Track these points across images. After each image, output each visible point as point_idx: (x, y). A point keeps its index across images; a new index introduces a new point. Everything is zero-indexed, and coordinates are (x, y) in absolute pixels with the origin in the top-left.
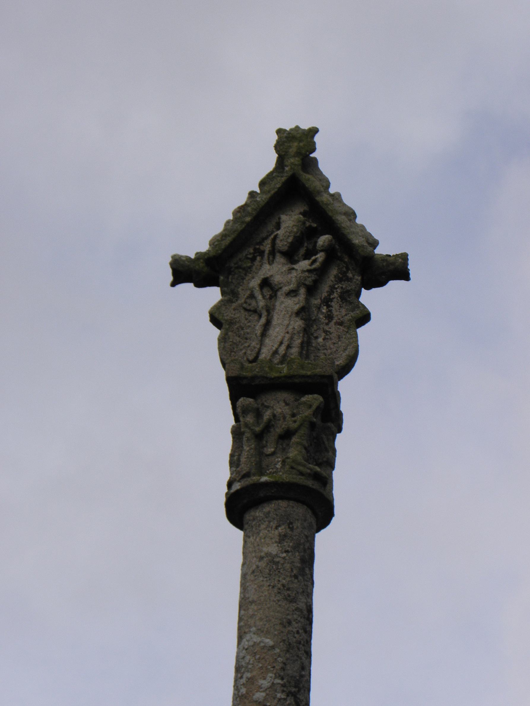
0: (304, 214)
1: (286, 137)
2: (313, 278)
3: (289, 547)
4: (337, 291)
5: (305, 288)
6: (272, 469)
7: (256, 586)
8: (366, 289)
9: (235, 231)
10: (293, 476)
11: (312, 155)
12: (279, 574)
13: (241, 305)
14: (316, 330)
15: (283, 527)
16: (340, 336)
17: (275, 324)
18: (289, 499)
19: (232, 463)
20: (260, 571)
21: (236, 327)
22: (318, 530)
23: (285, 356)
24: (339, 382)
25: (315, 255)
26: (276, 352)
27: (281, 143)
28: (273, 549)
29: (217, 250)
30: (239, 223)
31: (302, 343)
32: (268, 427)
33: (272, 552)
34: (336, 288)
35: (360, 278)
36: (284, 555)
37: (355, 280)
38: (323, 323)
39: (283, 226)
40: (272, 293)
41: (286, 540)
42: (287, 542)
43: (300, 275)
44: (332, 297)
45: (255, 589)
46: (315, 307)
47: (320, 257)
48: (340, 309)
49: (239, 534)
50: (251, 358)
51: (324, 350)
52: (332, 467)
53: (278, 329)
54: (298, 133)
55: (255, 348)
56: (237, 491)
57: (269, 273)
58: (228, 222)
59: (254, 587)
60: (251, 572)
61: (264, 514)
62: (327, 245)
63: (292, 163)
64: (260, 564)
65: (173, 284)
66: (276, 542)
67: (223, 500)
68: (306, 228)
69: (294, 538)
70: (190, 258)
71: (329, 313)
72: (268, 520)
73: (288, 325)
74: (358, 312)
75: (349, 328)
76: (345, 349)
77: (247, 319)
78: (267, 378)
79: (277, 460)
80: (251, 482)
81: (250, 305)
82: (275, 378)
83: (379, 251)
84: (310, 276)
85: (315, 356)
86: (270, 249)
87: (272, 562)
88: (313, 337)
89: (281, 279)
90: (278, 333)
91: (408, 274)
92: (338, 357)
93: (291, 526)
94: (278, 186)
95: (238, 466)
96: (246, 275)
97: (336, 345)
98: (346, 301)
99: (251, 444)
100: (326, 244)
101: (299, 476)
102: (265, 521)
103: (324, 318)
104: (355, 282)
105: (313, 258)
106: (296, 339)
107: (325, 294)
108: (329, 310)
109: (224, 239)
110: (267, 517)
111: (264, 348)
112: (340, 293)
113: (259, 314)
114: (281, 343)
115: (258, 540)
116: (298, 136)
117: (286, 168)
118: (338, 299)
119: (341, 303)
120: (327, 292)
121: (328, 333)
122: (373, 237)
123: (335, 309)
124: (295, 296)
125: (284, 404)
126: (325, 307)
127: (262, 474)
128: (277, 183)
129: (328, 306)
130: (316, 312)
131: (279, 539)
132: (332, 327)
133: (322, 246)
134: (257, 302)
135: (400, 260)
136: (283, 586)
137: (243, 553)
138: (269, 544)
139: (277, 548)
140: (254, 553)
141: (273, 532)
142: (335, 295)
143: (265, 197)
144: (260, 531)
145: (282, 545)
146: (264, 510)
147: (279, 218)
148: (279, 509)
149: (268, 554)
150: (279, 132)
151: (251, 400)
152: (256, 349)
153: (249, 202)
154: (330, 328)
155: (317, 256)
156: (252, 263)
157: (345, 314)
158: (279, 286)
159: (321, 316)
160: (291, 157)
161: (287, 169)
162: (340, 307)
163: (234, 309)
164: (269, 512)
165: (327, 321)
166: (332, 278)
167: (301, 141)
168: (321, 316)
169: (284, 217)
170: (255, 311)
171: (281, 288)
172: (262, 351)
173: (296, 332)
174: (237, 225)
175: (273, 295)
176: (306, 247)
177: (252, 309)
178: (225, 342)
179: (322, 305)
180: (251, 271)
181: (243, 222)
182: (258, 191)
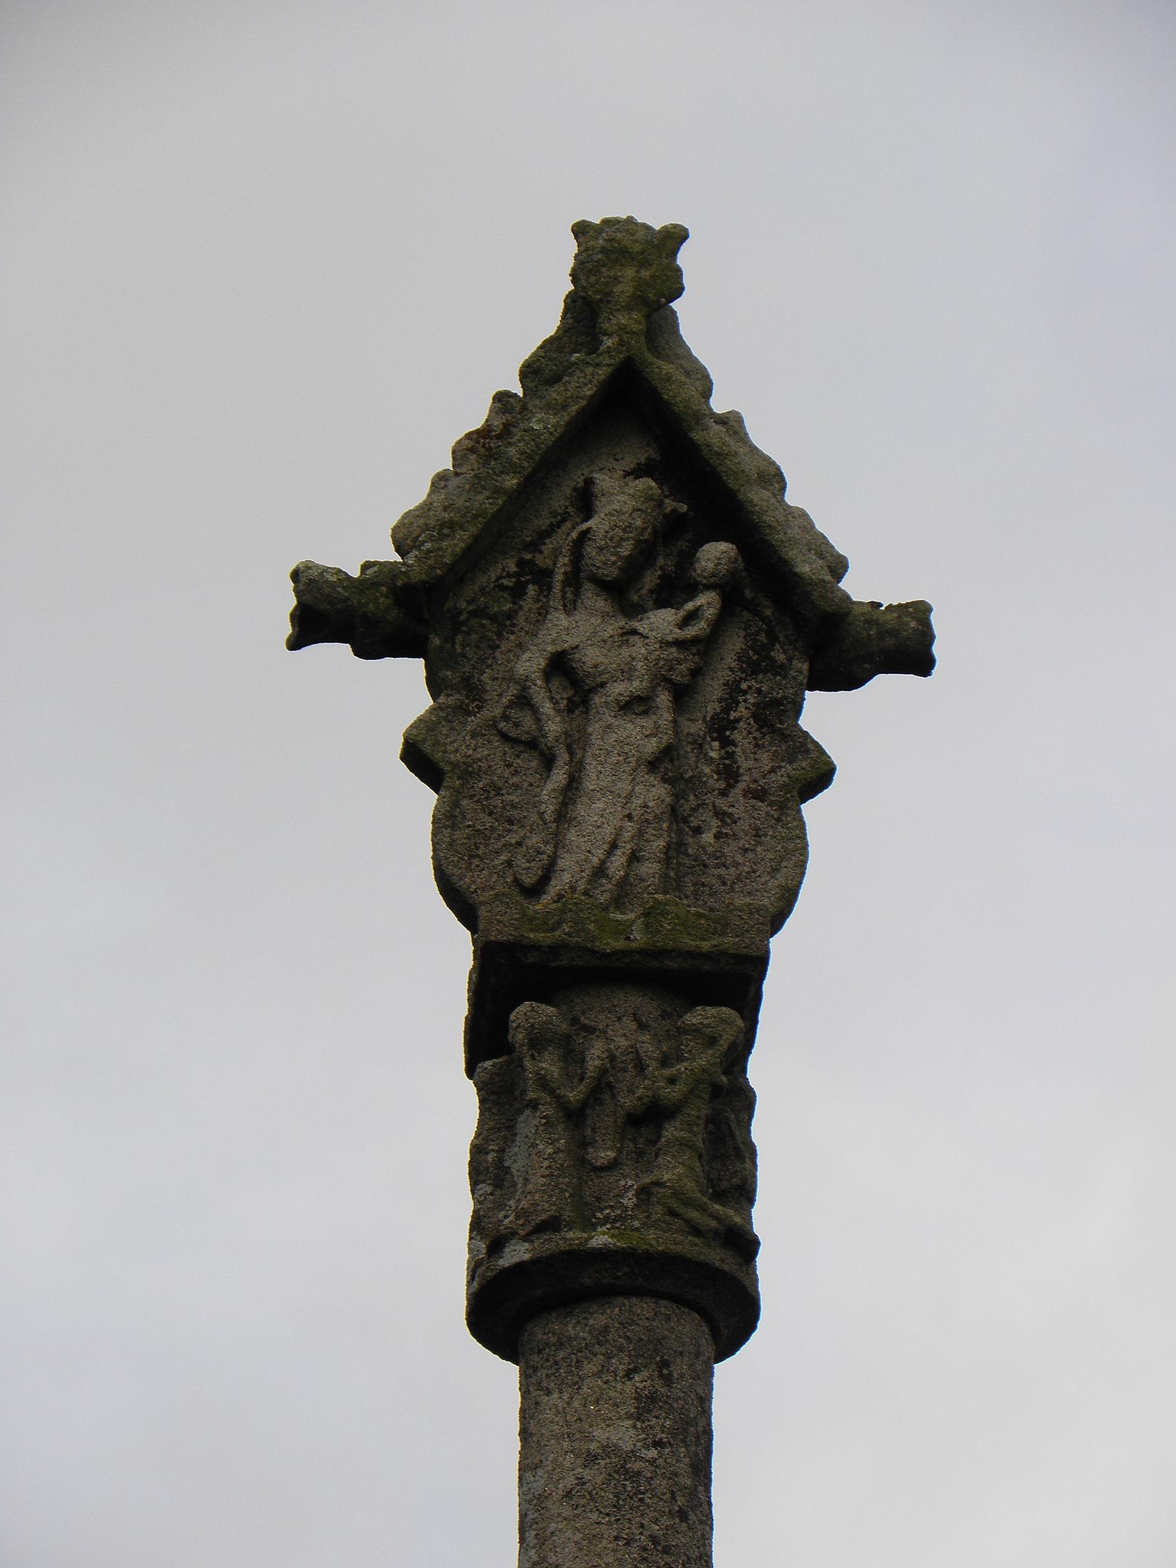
1: (603, 250)
2: (690, 665)
5: (670, 692)
7: (578, 1536)
9: (476, 516)
12: (642, 1508)
13: (493, 724)
14: (694, 810)
15: (645, 1373)
16: (760, 829)
17: (592, 787)
18: (658, 1295)
19: (477, 1173)
20: (590, 1493)
21: (481, 785)
23: (623, 883)
25: (692, 597)
26: (600, 871)
27: (589, 265)
28: (624, 1435)
29: (431, 568)
30: (487, 493)
31: (668, 847)
32: (602, 1087)
33: (621, 1443)
34: (745, 692)
36: (653, 1453)
37: (793, 673)
38: (713, 790)
40: (574, 696)
41: (655, 1413)
42: (657, 1417)
43: (657, 653)
44: (733, 715)
45: (576, 1543)
46: (692, 743)
48: (755, 753)
49: (510, 1372)
50: (528, 880)
51: (717, 866)
52: (751, 1201)
53: (600, 805)
54: (637, 241)
57: (568, 638)
60: (560, 1492)
61: (590, 1332)
62: (724, 571)
63: (622, 328)
64: (587, 1474)
65: (295, 643)
66: (629, 1416)
68: (665, 516)
69: (675, 1405)
71: (727, 762)
73: (629, 796)
74: (804, 764)
75: (782, 807)
76: (775, 870)
77: (509, 765)
78: (593, 952)
79: (622, 1183)
80: (563, 1246)
81: (516, 725)
82: (615, 953)
84: (682, 657)
85: (697, 884)
86: (569, 569)
87: (622, 1470)
88: (689, 827)
89: (601, 659)
90: (602, 816)
92: (757, 891)
93: (665, 1372)
94: (588, 391)
96: (499, 635)
97: (750, 855)
98: (773, 730)
99: (556, 1137)
100: (723, 569)
101: (690, 1238)
102: (595, 1355)
103: (716, 777)
105: (690, 606)
106: (652, 838)
107: (713, 708)
108: (727, 752)
109: (448, 536)
111: (565, 855)
112: (753, 704)
113: (542, 754)
114: (614, 846)
115: (576, 1404)
116: (637, 248)
117: (605, 338)
118: (749, 724)
119: (757, 734)
121: (729, 821)
122: (833, 547)
123: (744, 752)
124: (645, 713)
125: (634, 1026)
126: (716, 744)
127: (590, 1225)
128: (586, 384)
129: (725, 742)
130: (692, 758)
132: (738, 804)
133: (713, 575)
134: (538, 720)
135: (913, 624)
136: (654, 1539)
138: (610, 1419)
139: (632, 1432)
141: (619, 1386)
142: (742, 711)
144: (582, 1379)
145: (647, 1423)
146: (591, 1322)
148: (633, 1322)
149: (609, 1449)
150: (581, 230)
152: (545, 857)
153: (498, 422)
154: (733, 806)
156: (514, 603)
157: (769, 767)
158: (599, 680)
159: (707, 770)
160: (618, 310)
161: (608, 342)
162: (757, 745)
163: (474, 735)
164: (606, 1330)
165: (722, 785)
166: (730, 660)
167: (642, 265)
168: (707, 770)
170: (532, 744)
171: (603, 685)
172: (561, 863)
173: (650, 817)
174: (480, 497)
175: (576, 699)
176: (662, 568)
177: (524, 737)
178: (453, 827)
179: (708, 738)
180: (514, 625)
181: (497, 491)
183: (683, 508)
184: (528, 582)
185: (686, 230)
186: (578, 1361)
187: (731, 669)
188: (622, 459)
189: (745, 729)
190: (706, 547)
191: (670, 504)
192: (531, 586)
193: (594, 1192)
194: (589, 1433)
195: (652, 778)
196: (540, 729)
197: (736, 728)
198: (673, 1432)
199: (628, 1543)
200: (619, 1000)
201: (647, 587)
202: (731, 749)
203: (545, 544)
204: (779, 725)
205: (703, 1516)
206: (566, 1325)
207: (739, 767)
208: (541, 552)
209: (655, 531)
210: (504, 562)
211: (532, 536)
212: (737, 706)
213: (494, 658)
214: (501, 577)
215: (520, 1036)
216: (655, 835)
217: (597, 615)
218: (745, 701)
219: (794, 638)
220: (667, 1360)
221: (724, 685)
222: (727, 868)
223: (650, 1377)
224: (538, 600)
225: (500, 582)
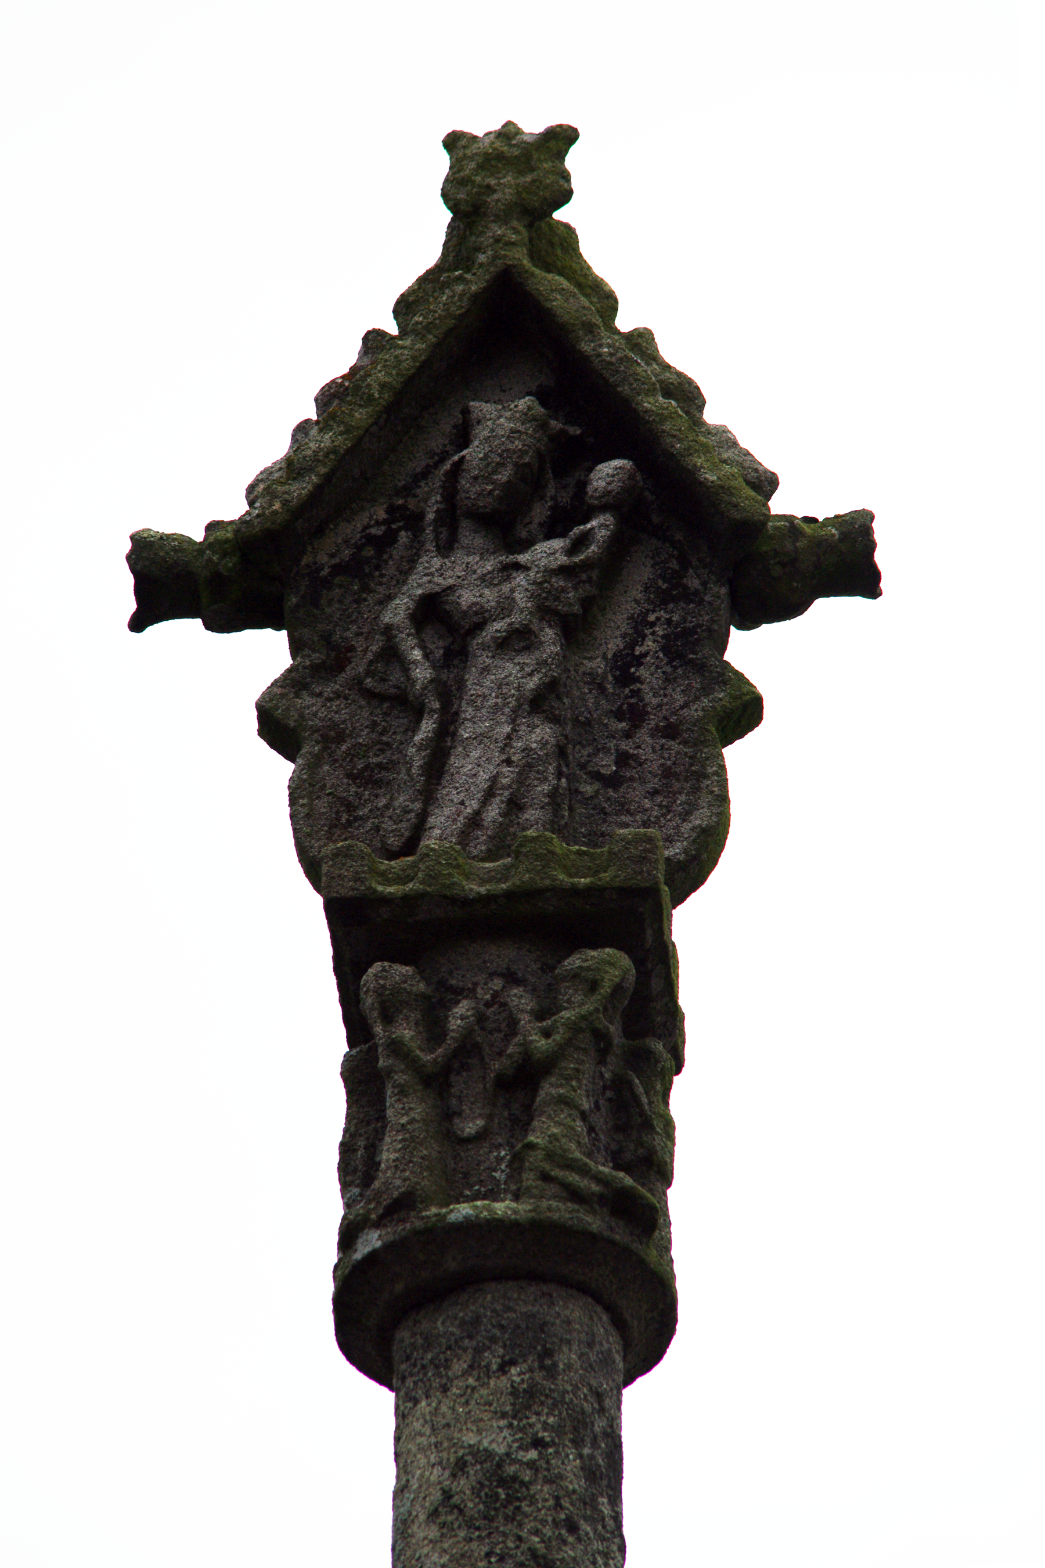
0: (542, 396)
3: (545, 1430)
4: (653, 633)
6: (481, 1182)
8: (740, 627)
10: (550, 1202)
11: (559, 215)
13: (357, 683)
22: (629, 1380)
24: (674, 912)
25: (585, 523)
26: (475, 821)
33: (494, 1446)
34: (653, 624)
35: (723, 591)
36: (533, 1454)
39: (482, 432)
41: (536, 1408)
42: (538, 1414)
44: (638, 650)
47: (600, 526)
49: (383, 1399)
55: (406, 811)
56: (372, 1257)
58: (302, 429)
59: (442, 1561)
65: (138, 624)
67: (328, 1288)
70: (190, 541)
71: (633, 701)
72: (474, 1343)
83: (779, 505)
91: (875, 576)
95: (367, 1180)
101: (569, 1204)
102: (465, 1350)
104: (709, 603)
105: (578, 530)
107: (614, 645)
108: (631, 691)
110: (470, 1337)
112: (663, 637)
114: (489, 794)
118: (658, 658)
119: (668, 669)
120: (624, 636)
124: (527, 649)
131: (513, 1404)
137: (397, 1455)
140: (434, 1450)
142: (650, 644)
143: (416, 347)
147: (466, 412)
149: (483, 1456)
151: (407, 970)
155: (589, 526)
162: (667, 680)
166: (637, 592)
169: (481, 408)
172: (431, 820)
180: (382, 576)
182: (393, 329)
183: (575, 431)
184: (400, 529)
185: (575, 131)
186: (446, 1360)
187: (637, 602)
188: (510, 389)
189: (653, 664)
190: (600, 467)
191: (555, 425)
192: (403, 533)
193: (462, 1167)
194: (459, 1439)
195: (535, 719)
196: (408, 678)
197: (642, 664)
198: (558, 1430)
199: (502, 1559)
200: (491, 955)
201: (536, 521)
202: (635, 687)
203: (420, 487)
204: (691, 656)
205: (607, 1532)
206: (435, 1323)
207: (645, 706)
208: (415, 496)
209: (540, 455)
210: (372, 510)
211: (405, 480)
212: (644, 640)
213: (359, 613)
214: (368, 527)
215: (369, 1000)
216: (539, 779)
217: (475, 554)
218: (653, 633)
219: (708, 560)
220: (550, 1349)
221: (628, 619)
222: (632, 815)
223: (531, 1370)
224: (411, 547)
225: (368, 531)
